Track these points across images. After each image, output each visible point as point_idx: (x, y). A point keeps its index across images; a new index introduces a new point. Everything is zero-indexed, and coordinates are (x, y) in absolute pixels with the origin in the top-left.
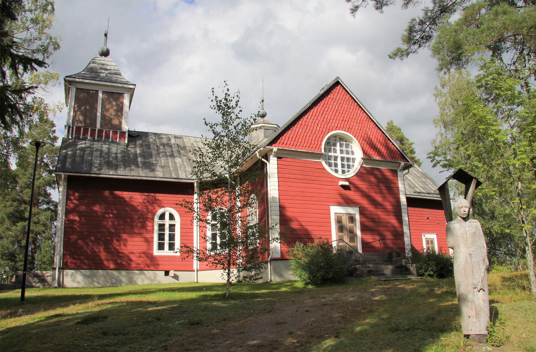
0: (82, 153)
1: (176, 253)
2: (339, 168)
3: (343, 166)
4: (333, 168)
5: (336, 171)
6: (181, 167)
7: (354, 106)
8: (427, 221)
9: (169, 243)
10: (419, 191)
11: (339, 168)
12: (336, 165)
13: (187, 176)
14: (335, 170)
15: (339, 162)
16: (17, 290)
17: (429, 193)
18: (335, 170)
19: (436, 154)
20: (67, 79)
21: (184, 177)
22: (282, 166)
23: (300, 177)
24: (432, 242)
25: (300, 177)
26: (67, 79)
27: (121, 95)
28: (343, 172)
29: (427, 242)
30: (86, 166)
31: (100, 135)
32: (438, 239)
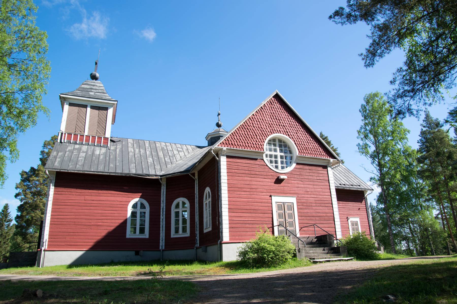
0: (70, 154)
1: (188, 234)
2: (280, 165)
3: (282, 163)
4: (274, 164)
5: (277, 167)
6: (151, 165)
7: (284, 115)
8: (360, 207)
9: (186, 224)
10: (344, 183)
11: (280, 165)
12: (276, 162)
13: (80, 157)
14: (270, 160)
15: (279, 160)
16: (52, 265)
17: (352, 185)
18: (270, 160)
19: (284, 262)
20: (61, 95)
21: (154, 173)
22: (231, 163)
23: (247, 172)
24: (357, 224)
25: (247, 172)
26: (61, 95)
27: (106, 109)
28: (283, 168)
29: (353, 224)
30: (72, 165)
31: (88, 140)
32: (360, 221)
